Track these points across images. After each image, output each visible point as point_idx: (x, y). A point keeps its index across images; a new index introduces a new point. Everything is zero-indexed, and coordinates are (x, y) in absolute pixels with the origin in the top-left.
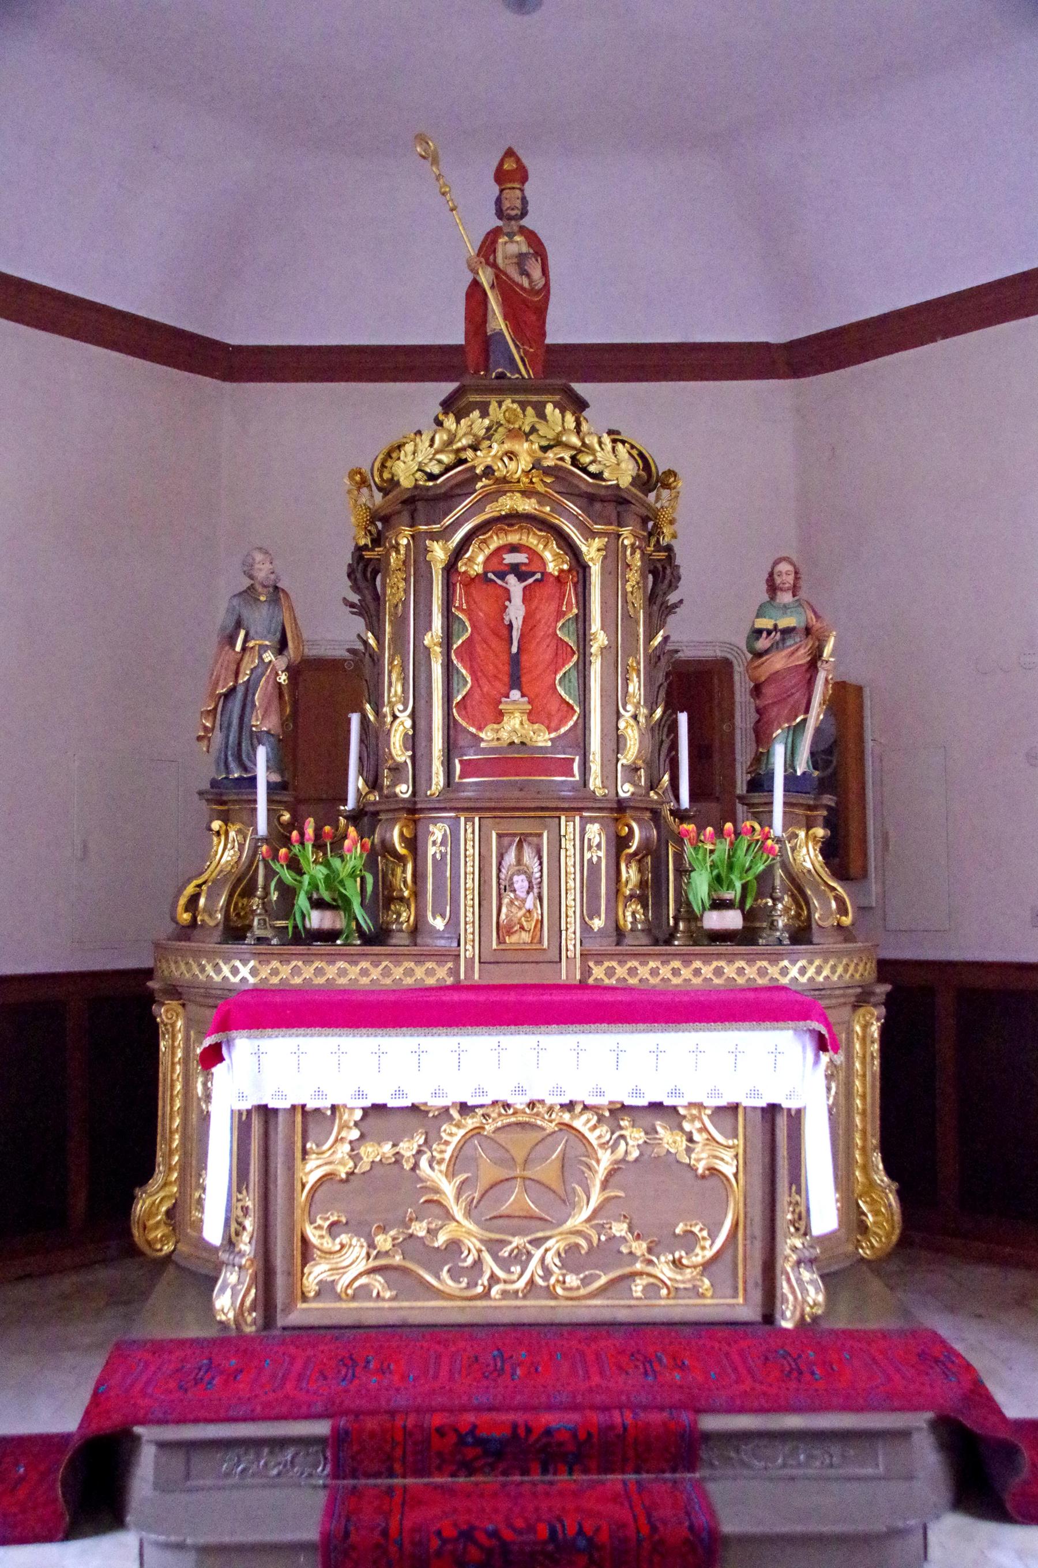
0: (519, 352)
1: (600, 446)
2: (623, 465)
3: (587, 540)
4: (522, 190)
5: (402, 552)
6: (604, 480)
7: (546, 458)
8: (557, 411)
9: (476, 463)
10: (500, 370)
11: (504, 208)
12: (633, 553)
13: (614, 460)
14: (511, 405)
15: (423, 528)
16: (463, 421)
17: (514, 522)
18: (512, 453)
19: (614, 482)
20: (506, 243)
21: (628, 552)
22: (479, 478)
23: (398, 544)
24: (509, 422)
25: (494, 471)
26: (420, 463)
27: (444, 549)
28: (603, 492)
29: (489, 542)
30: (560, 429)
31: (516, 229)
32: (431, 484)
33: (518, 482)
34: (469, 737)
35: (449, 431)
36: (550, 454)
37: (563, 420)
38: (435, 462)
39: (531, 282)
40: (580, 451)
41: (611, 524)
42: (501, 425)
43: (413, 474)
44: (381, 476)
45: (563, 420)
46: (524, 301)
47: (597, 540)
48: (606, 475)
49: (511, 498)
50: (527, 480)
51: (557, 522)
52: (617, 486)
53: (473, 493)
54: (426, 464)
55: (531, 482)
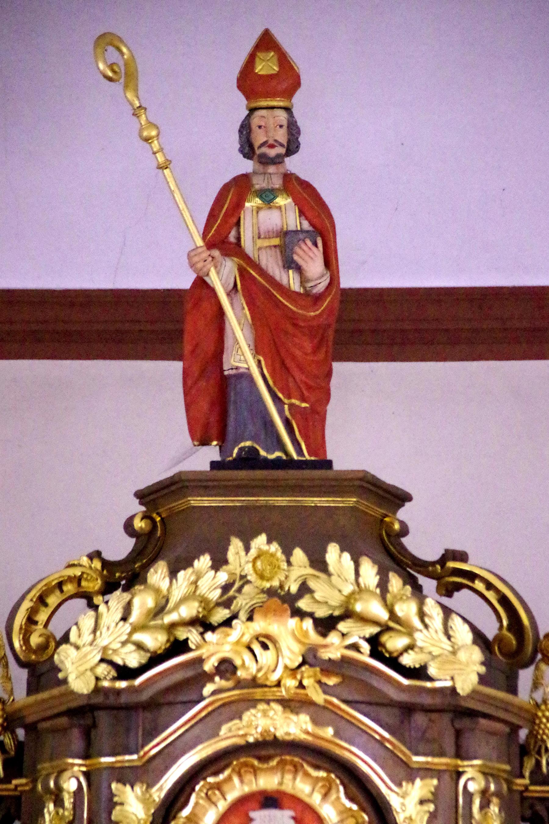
0: (281, 412)
1: (423, 621)
2: (462, 656)
3: (400, 785)
4: (288, 110)
5: (68, 802)
6: (430, 679)
7: (325, 646)
8: (346, 556)
9: (203, 652)
10: (248, 443)
11: (256, 144)
12: (485, 805)
13: (446, 645)
14: (265, 547)
15: (106, 760)
16: (181, 575)
17: (271, 752)
18: (268, 637)
19: (449, 684)
20: (259, 209)
21: (477, 802)
22: (209, 678)
23: (59, 789)
24: (262, 577)
25: (235, 669)
26: (105, 649)
27: (145, 801)
28: (427, 700)
29: (225, 788)
30: (348, 589)
31: (277, 182)
32: (122, 684)
33: (278, 684)
34: (129, 770)
35: (157, 591)
36: (333, 638)
37: (357, 573)
38: (131, 647)
39: (303, 280)
40: (386, 629)
41: (442, 754)
42: (248, 582)
43: (92, 669)
44: (26, 640)
45: (357, 573)
46: (293, 319)
47: (418, 781)
48: (432, 671)
49: (265, 714)
50: (294, 683)
51: (347, 755)
52: (453, 690)
53: (198, 702)
54: (115, 651)
55: (301, 686)
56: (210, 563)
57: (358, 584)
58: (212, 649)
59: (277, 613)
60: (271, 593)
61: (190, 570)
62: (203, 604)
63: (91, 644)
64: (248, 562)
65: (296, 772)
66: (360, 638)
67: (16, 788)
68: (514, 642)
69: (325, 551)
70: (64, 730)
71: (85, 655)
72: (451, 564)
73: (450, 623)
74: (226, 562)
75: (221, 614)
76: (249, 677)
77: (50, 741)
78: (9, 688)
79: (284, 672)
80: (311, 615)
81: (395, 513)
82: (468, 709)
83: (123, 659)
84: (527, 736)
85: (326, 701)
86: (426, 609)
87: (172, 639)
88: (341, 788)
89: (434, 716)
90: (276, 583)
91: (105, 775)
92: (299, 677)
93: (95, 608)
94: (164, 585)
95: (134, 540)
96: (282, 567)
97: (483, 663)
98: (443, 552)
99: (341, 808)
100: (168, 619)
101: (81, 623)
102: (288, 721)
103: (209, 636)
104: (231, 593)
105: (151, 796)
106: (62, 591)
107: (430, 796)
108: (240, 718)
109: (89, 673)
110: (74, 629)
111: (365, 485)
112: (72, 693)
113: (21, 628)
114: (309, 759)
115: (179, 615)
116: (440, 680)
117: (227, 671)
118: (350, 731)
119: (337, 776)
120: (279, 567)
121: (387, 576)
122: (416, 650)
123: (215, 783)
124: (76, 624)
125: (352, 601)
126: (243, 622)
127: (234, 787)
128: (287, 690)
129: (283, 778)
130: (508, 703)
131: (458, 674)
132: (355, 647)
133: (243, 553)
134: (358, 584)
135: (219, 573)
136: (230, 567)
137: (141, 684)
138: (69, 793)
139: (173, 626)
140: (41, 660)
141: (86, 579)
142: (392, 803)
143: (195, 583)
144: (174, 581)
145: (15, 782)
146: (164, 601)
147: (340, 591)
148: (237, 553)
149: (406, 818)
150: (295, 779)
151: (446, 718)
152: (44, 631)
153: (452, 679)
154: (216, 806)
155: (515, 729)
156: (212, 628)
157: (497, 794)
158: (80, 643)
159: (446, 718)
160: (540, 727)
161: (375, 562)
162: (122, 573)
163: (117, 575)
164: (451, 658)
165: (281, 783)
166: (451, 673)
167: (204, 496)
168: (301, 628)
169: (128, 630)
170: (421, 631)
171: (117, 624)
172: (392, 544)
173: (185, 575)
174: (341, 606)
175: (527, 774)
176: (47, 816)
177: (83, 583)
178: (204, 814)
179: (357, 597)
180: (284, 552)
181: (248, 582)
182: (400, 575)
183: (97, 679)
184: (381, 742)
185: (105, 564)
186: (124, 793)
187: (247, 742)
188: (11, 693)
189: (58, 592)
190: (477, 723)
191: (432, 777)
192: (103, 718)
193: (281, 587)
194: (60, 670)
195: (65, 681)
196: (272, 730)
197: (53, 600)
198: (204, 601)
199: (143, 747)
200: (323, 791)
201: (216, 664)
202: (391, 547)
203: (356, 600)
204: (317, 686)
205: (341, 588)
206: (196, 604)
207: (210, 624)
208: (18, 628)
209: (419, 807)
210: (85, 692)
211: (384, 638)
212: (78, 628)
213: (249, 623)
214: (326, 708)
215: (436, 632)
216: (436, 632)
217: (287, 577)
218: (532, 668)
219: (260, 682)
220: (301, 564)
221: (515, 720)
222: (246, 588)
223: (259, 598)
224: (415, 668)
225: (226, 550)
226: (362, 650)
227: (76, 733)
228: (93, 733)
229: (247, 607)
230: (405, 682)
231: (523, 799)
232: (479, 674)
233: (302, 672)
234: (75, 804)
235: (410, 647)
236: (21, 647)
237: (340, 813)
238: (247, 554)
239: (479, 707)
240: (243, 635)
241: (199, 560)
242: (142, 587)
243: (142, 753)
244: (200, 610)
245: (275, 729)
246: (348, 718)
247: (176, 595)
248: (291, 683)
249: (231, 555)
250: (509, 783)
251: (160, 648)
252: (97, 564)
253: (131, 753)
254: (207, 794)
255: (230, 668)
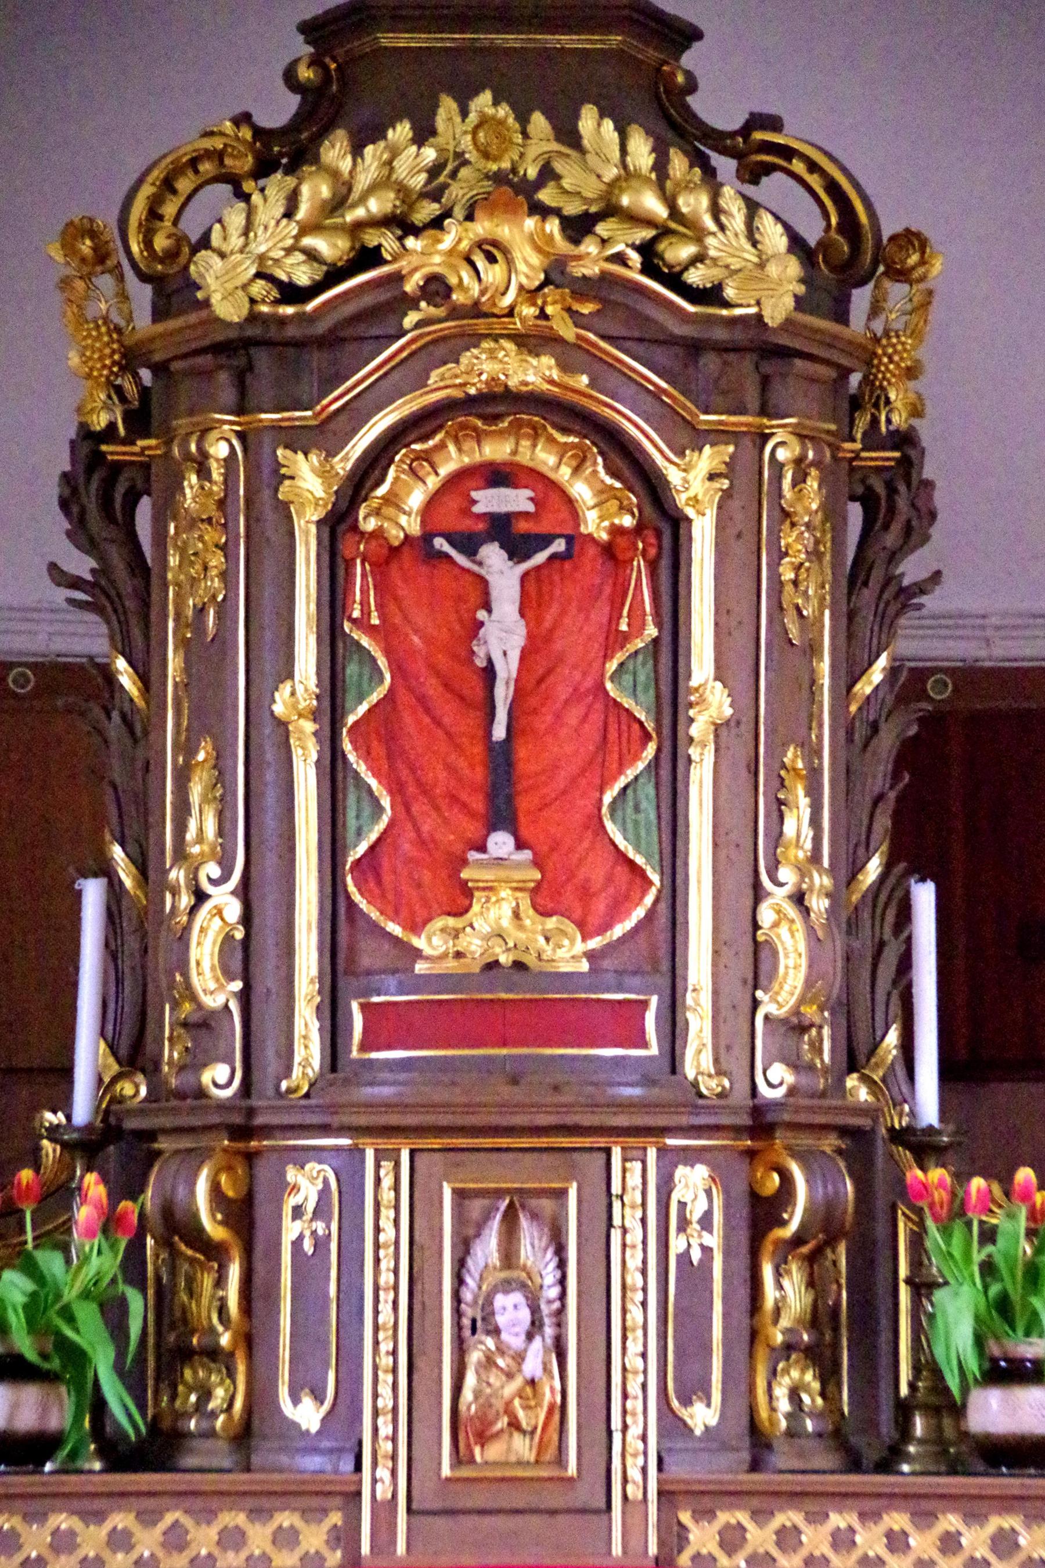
2: (773, 270)
3: (681, 454)
6: (727, 305)
7: (579, 258)
8: (608, 125)
9: (403, 265)
12: (800, 479)
13: (750, 255)
14: (490, 111)
16: (369, 150)
17: (501, 409)
18: (495, 244)
19: (753, 310)
22: (411, 303)
23: (204, 455)
24: (486, 155)
25: (449, 290)
26: (262, 258)
27: (325, 473)
28: (720, 334)
29: (437, 458)
30: (611, 173)
32: (289, 310)
33: (511, 312)
35: (334, 174)
36: (590, 247)
37: (624, 151)
38: (300, 257)
40: (665, 232)
41: (741, 411)
42: (466, 163)
43: (245, 287)
44: (148, 244)
45: (624, 151)
47: (707, 449)
48: (730, 293)
49: (492, 356)
54: (276, 261)
55: (543, 315)
56: (410, 135)
57: (624, 165)
58: (415, 260)
59: (509, 209)
60: (499, 178)
61: (382, 144)
62: (401, 195)
63: (241, 251)
64: (465, 133)
65: (535, 438)
66: (627, 245)
67: (142, 453)
68: (846, 248)
69: (576, 116)
70: (206, 374)
71: (235, 267)
72: (759, 136)
73: (757, 223)
74: (433, 133)
75: (428, 210)
76: (469, 302)
77: (186, 390)
78: (126, 311)
79: (518, 295)
80: (557, 212)
81: (677, 59)
82: (777, 345)
83: (288, 274)
84: (860, 383)
85: (579, 337)
86: (722, 203)
87: (357, 246)
88: (600, 460)
89: (732, 357)
90: (506, 165)
91: (267, 439)
92: (540, 302)
93: (246, 198)
94: (345, 165)
95: (297, 98)
96: (515, 140)
97: (802, 281)
98: (747, 116)
99: (599, 486)
100: (352, 216)
101: (226, 219)
102: (524, 364)
103: (411, 242)
104: (442, 179)
105: (332, 467)
106: (196, 172)
107: (723, 468)
108: (457, 362)
109: (240, 293)
110: (217, 227)
111: (635, 16)
112: (218, 320)
113: (140, 224)
114: (556, 419)
115: (368, 210)
116: (741, 306)
117: (438, 293)
118: (613, 380)
119: (594, 443)
120: (510, 139)
121: (667, 155)
122: (707, 262)
123: (422, 451)
124: (220, 221)
125: (617, 192)
126: (460, 223)
127: (449, 458)
128: (523, 320)
129: (517, 444)
130: (835, 337)
131: (767, 297)
132: (620, 259)
133: (458, 119)
134: (625, 166)
135: (422, 150)
136: (440, 140)
137: (316, 310)
138: (217, 460)
139: (359, 226)
140: (171, 272)
141: (232, 155)
142: (670, 478)
143: (389, 163)
144: (359, 160)
145: (141, 443)
146: (344, 190)
147: (599, 176)
148: (450, 119)
149: (689, 499)
150: (534, 446)
151: (747, 363)
152: (174, 230)
153: (758, 303)
154: (424, 483)
155: (845, 373)
156: (415, 231)
157: (817, 464)
158: (226, 248)
159: (747, 363)
160: (879, 371)
161: (648, 132)
162: (282, 147)
163: (276, 149)
164: (757, 273)
165: (515, 452)
166: (757, 294)
167: (401, 32)
168: (543, 230)
169: (295, 232)
170: (714, 234)
171: (278, 222)
172: (673, 106)
173: (375, 150)
174: (601, 198)
175: (859, 436)
176: (188, 491)
177: (228, 161)
178: (409, 494)
179: (624, 184)
180: (517, 118)
181: (466, 163)
182: (686, 153)
183: (253, 301)
184: (657, 394)
185: (259, 132)
186: (295, 462)
187: (467, 394)
188: (130, 319)
189: (190, 174)
190: (792, 365)
191: (727, 444)
192: (262, 359)
193: (514, 170)
194: (199, 288)
195: (206, 303)
196: (502, 377)
197: (184, 185)
198: (402, 189)
199: (318, 402)
200: (574, 463)
201: (421, 283)
202: (672, 111)
203: (622, 190)
204: (566, 315)
205: (599, 172)
206: (392, 195)
207: (413, 224)
208: (136, 224)
209: (708, 484)
210: (236, 320)
211: (661, 246)
212: (224, 228)
213: (468, 224)
214: (580, 346)
215: (736, 235)
216: (736, 235)
217: (522, 155)
218: (871, 285)
219: (485, 309)
220: (542, 136)
221: (845, 361)
222: (464, 172)
223: (482, 187)
224: (705, 289)
225: (434, 113)
226: (630, 263)
227: (223, 377)
228: (249, 379)
229: (464, 200)
230: (691, 308)
231: (852, 470)
232: (795, 296)
233: (545, 296)
234: (226, 477)
235: (699, 259)
236: (141, 252)
237: (599, 492)
238: (463, 121)
239: (797, 344)
240: (460, 240)
241: (394, 129)
242: (314, 168)
243: (318, 408)
244: (398, 203)
245: (506, 376)
246: (611, 361)
247: (363, 180)
248: (529, 311)
249: (441, 123)
250: (835, 448)
251: (340, 259)
252: (246, 133)
253: (306, 409)
254: (410, 466)
255: (442, 289)
